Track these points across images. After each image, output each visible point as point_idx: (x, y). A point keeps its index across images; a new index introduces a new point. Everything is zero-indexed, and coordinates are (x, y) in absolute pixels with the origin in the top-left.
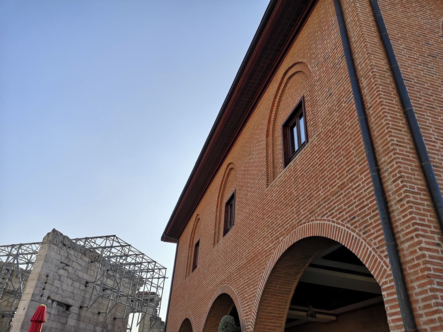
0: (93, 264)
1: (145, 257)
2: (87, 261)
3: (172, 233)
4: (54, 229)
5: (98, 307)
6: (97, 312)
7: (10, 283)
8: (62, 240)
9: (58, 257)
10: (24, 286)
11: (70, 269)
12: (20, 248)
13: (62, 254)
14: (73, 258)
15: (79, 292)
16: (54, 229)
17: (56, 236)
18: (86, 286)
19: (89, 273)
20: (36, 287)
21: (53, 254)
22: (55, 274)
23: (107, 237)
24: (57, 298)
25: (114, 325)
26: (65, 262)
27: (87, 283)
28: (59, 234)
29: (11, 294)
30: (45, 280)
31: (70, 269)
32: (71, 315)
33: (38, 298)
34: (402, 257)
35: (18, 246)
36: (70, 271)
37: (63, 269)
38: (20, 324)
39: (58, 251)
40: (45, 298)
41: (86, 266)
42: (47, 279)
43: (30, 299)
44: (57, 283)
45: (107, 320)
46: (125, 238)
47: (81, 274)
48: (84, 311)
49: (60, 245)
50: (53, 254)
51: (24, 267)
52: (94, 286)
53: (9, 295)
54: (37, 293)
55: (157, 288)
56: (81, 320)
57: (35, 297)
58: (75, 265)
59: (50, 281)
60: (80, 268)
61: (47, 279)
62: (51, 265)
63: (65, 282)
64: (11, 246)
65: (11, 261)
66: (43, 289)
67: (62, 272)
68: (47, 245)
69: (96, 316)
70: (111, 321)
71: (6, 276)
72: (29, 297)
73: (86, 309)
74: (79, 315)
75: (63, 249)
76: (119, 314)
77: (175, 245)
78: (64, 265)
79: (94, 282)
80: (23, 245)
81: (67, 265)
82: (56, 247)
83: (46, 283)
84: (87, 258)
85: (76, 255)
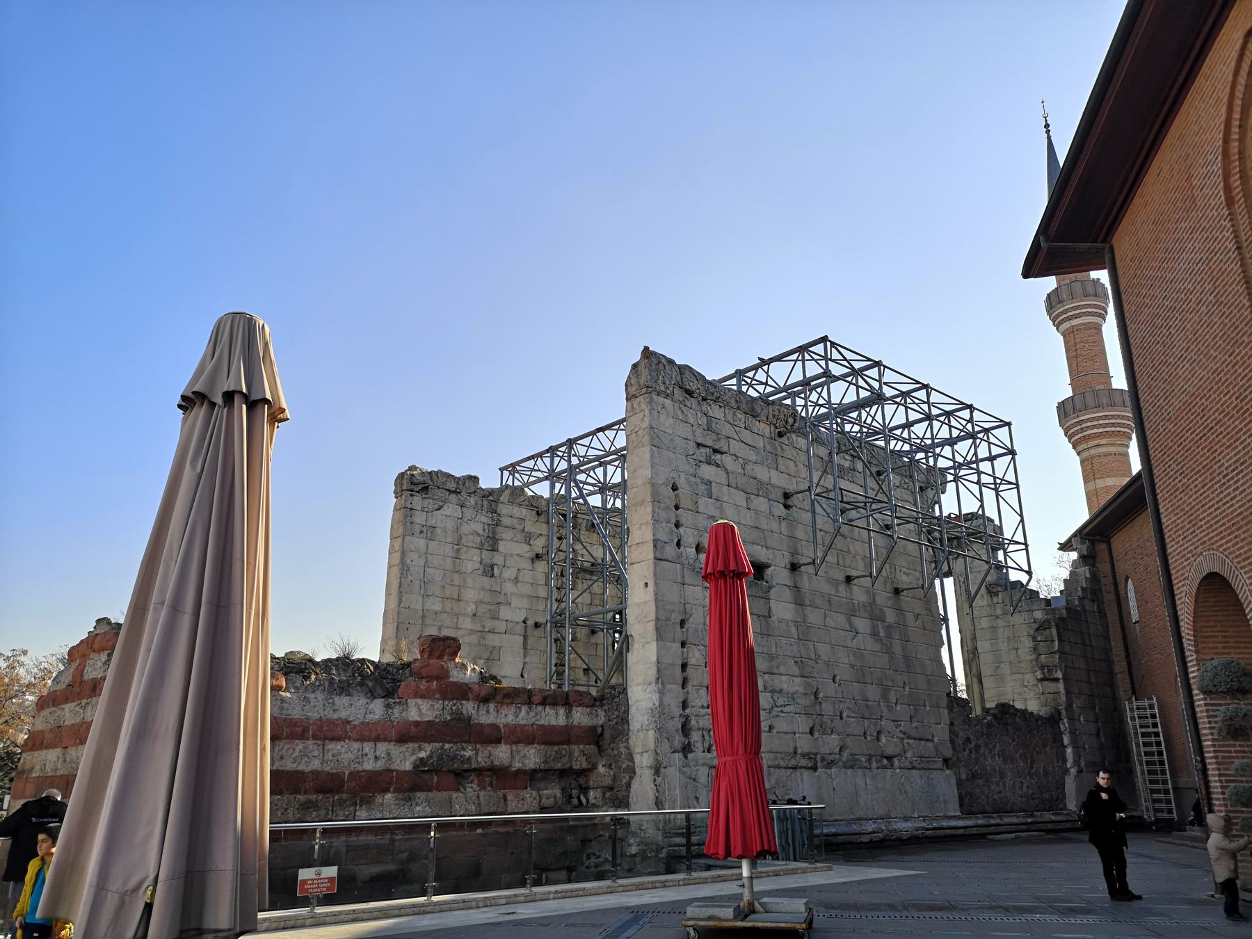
0: (784, 439)
1: (934, 397)
2: (767, 434)
3: (1080, 225)
4: (646, 348)
5: (841, 563)
6: (842, 578)
7: (578, 547)
8: (679, 378)
9: (684, 430)
11: (727, 460)
13: (691, 421)
14: (727, 430)
15: (774, 525)
16: (646, 348)
17: (658, 370)
18: (787, 507)
19: (782, 467)
20: (656, 521)
21: (667, 423)
22: (692, 479)
23: (803, 349)
25: (900, 610)
26: (709, 443)
27: (787, 496)
28: (664, 361)
29: (592, 573)
30: (671, 501)
31: (727, 460)
32: (773, 590)
33: (670, 551)
35: (563, 449)
36: (730, 468)
38: (651, 627)
39: (679, 413)
40: (688, 550)
41: (768, 448)
42: (677, 496)
43: (651, 556)
44: (705, 505)
45: (877, 598)
46: (860, 340)
47: (762, 473)
48: (805, 577)
49: (678, 394)
50: (667, 423)
52: (813, 501)
53: (588, 577)
54: (663, 537)
55: (996, 490)
56: (807, 602)
57: (663, 548)
58: (735, 446)
59: (686, 502)
60: (753, 457)
61: (677, 496)
62: (673, 456)
63: (725, 499)
64: (547, 451)
65: (563, 492)
66: (677, 525)
67: (707, 471)
68: (641, 399)
69: (842, 588)
70: (889, 598)
71: (563, 532)
72: (648, 552)
73: (810, 569)
74: (796, 589)
75: (689, 404)
76: (904, 578)
79: (809, 489)
81: (716, 451)
82: (668, 402)
83: (677, 508)
84: (763, 425)
85: (730, 418)
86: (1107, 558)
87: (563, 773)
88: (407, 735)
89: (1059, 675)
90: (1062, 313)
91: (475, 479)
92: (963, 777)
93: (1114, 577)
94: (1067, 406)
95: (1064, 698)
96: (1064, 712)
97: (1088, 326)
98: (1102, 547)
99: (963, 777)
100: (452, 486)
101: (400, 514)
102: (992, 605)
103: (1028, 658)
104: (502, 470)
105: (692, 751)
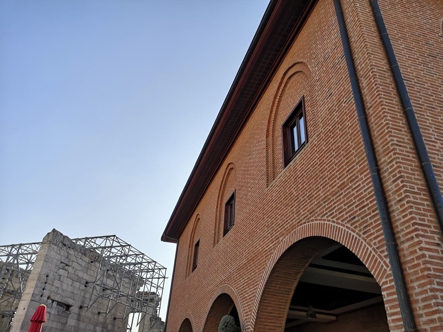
0: (93, 264)
1: (145, 257)
2: (87, 261)
3: (172, 233)
4: (54, 229)
5: (98, 307)
6: (97, 312)
7: (10, 283)
8: (62, 240)
9: (58, 257)
10: (24, 286)
11: (70, 269)
12: (20, 248)
13: (62, 254)
14: (73, 258)
15: (79, 292)
16: (54, 229)
17: (56, 236)
18: (86, 286)
19: (89, 273)
20: (36, 287)
21: (53, 254)
22: (55, 274)
23: (107, 237)
24: (57, 298)
25: (114, 325)
26: (65, 262)
27: (87, 283)
28: (59, 234)
29: (11, 294)
30: (45, 280)
31: (70, 269)
32: (71, 315)
33: (38, 298)
35: (18, 246)
36: (70, 271)
37: (63, 269)
38: (20, 324)
39: (58, 251)
40: (45, 298)
41: (86, 266)
42: (47, 279)
43: (30, 299)
44: (57, 283)
45: (107, 320)
46: (125, 238)
47: (81, 274)
48: (84, 311)
49: (60, 245)
50: (53, 254)
51: (24, 267)
52: (94, 286)
53: (9, 295)
54: (37, 293)
55: (157, 288)
56: (81, 320)
57: (35, 297)
58: (75, 265)
59: (50, 281)
60: (80, 268)
61: (47, 279)
62: (51, 265)
63: (65, 282)
64: (11, 246)
65: (11, 261)
66: (43, 289)
67: (62, 272)
68: (47, 245)
69: (96, 316)
70: (111, 321)
71: (6, 276)
72: (29, 297)
73: (86, 309)
74: (79, 315)
75: (63, 249)
76: (119, 314)
77: (175, 245)
78: (64, 265)
79: (94, 282)
80: (23, 245)
81: (67, 265)
82: (56, 247)
83: (46, 283)
84: (87, 258)
85: (76, 255)
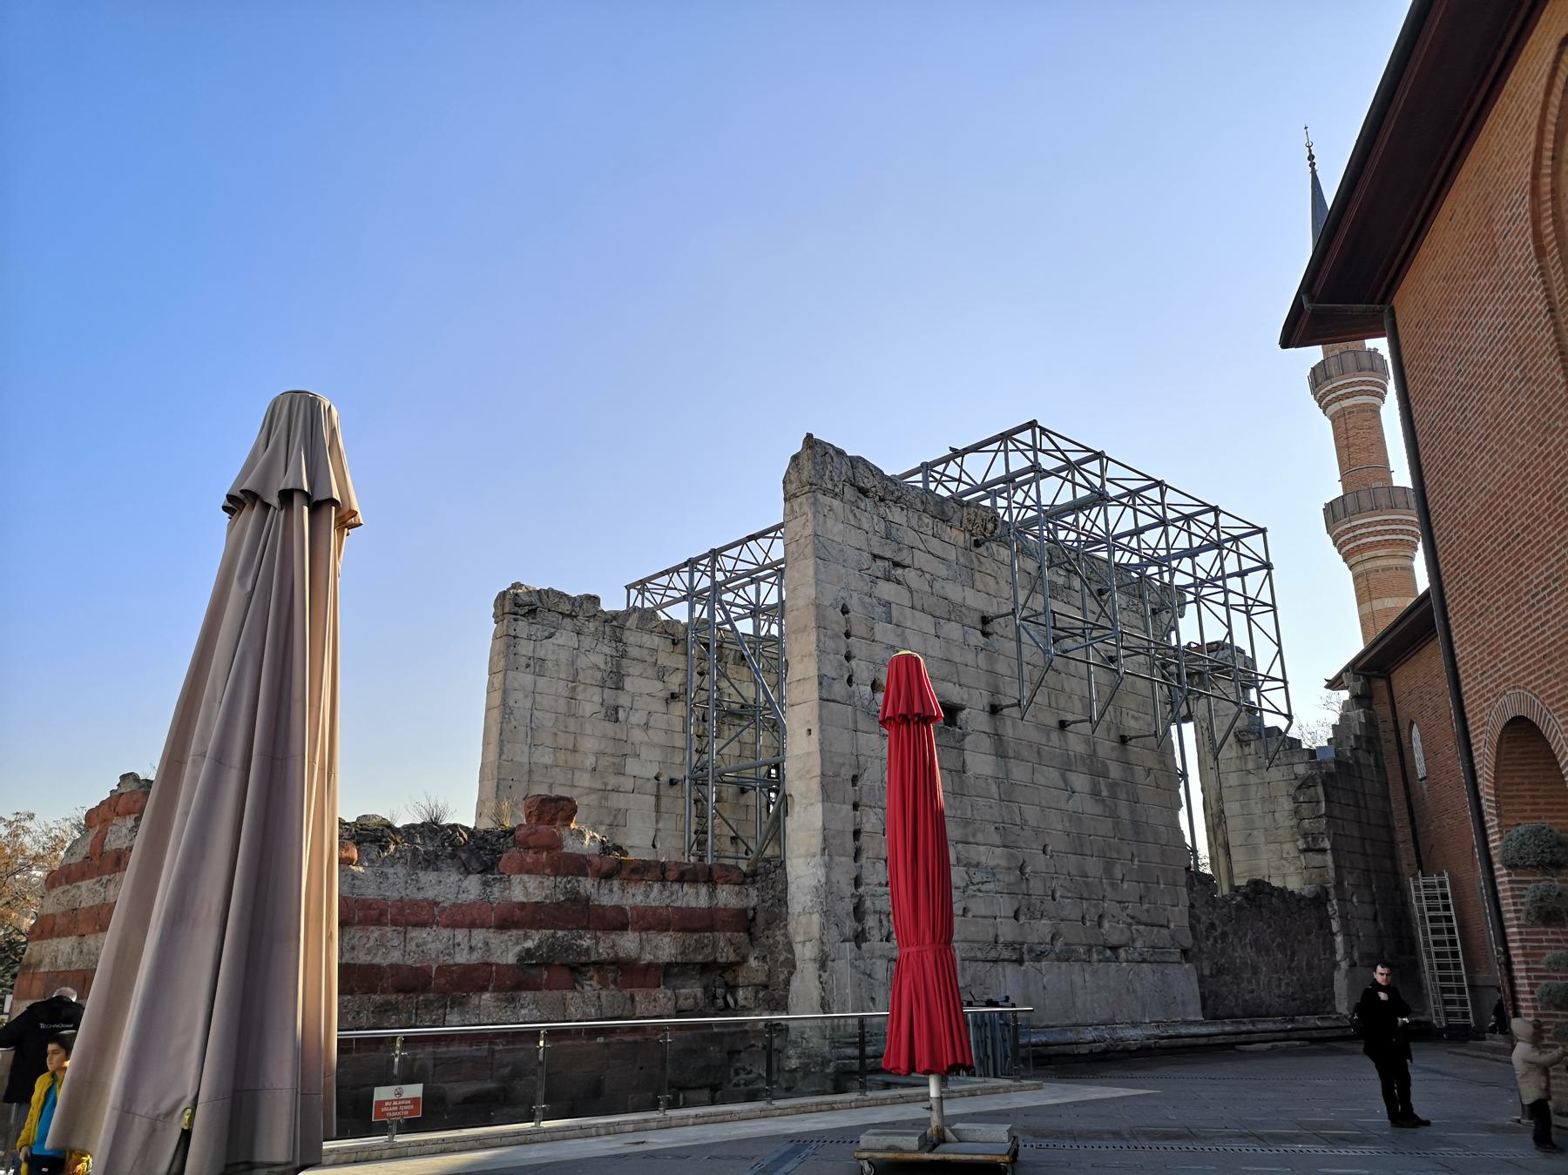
0: (982, 550)
1: (1170, 497)
2: (961, 543)
3: (1353, 281)
4: (809, 436)
5: (1053, 704)
6: (1054, 723)
7: (724, 684)
8: (850, 473)
9: (856, 539)
11: (910, 575)
13: (866, 526)
14: (910, 538)
15: (970, 657)
16: (809, 436)
17: (824, 463)
18: (985, 634)
19: (979, 585)
20: (821, 652)
21: (835, 529)
22: (867, 599)
23: (1005, 437)
25: (1127, 764)
26: (888, 555)
27: (985, 620)
28: (831, 451)
29: (741, 717)
30: (840, 627)
31: (910, 575)
32: (968, 739)
33: (840, 689)
34: (879, 901)
35: (705, 562)
36: (914, 585)
38: (815, 784)
39: (851, 517)
40: (862, 688)
41: (962, 560)
42: (848, 621)
43: (816, 695)
44: (883, 631)
45: (1099, 749)
46: (1077, 425)
47: (955, 592)
48: (1009, 722)
49: (849, 493)
50: (835, 529)
52: (1018, 628)
53: (737, 722)
54: (830, 671)
55: (1247, 613)
56: (1011, 754)
57: (830, 686)
58: (921, 559)
59: (859, 628)
60: (944, 572)
61: (848, 621)
62: (843, 571)
63: (908, 624)
64: (686, 564)
65: (705, 616)
66: (848, 657)
67: (886, 590)
68: (803, 499)
69: (1055, 735)
70: (1113, 749)
71: (705, 665)
72: (811, 691)
73: (1015, 712)
74: (997, 737)
75: (862, 505)
76: (1132, 723)
79: (1013, 612)
81: (896, 564)
82: (836, 503)
83: (848, 635)
84: (955, 532)
85: (914, 523)
86: (1386, 698)
87: (705, 967)
88: (510, 919)
89: (1327, 844)
90: (1330, 392)
91: (595, 600)
92: (1207, 972)
93: (1396, 722)
94: (1336, 508)
95: (1332, 874)
96: (1332, 891)
97: (1363, 408)
98: (1380, 684)
99: (1207, 972)
100: (566, 608)
101: (500, 644)
102: (1243, 758)
103: (1287, 823)
104: (628, 588)
105: (866, 940)
